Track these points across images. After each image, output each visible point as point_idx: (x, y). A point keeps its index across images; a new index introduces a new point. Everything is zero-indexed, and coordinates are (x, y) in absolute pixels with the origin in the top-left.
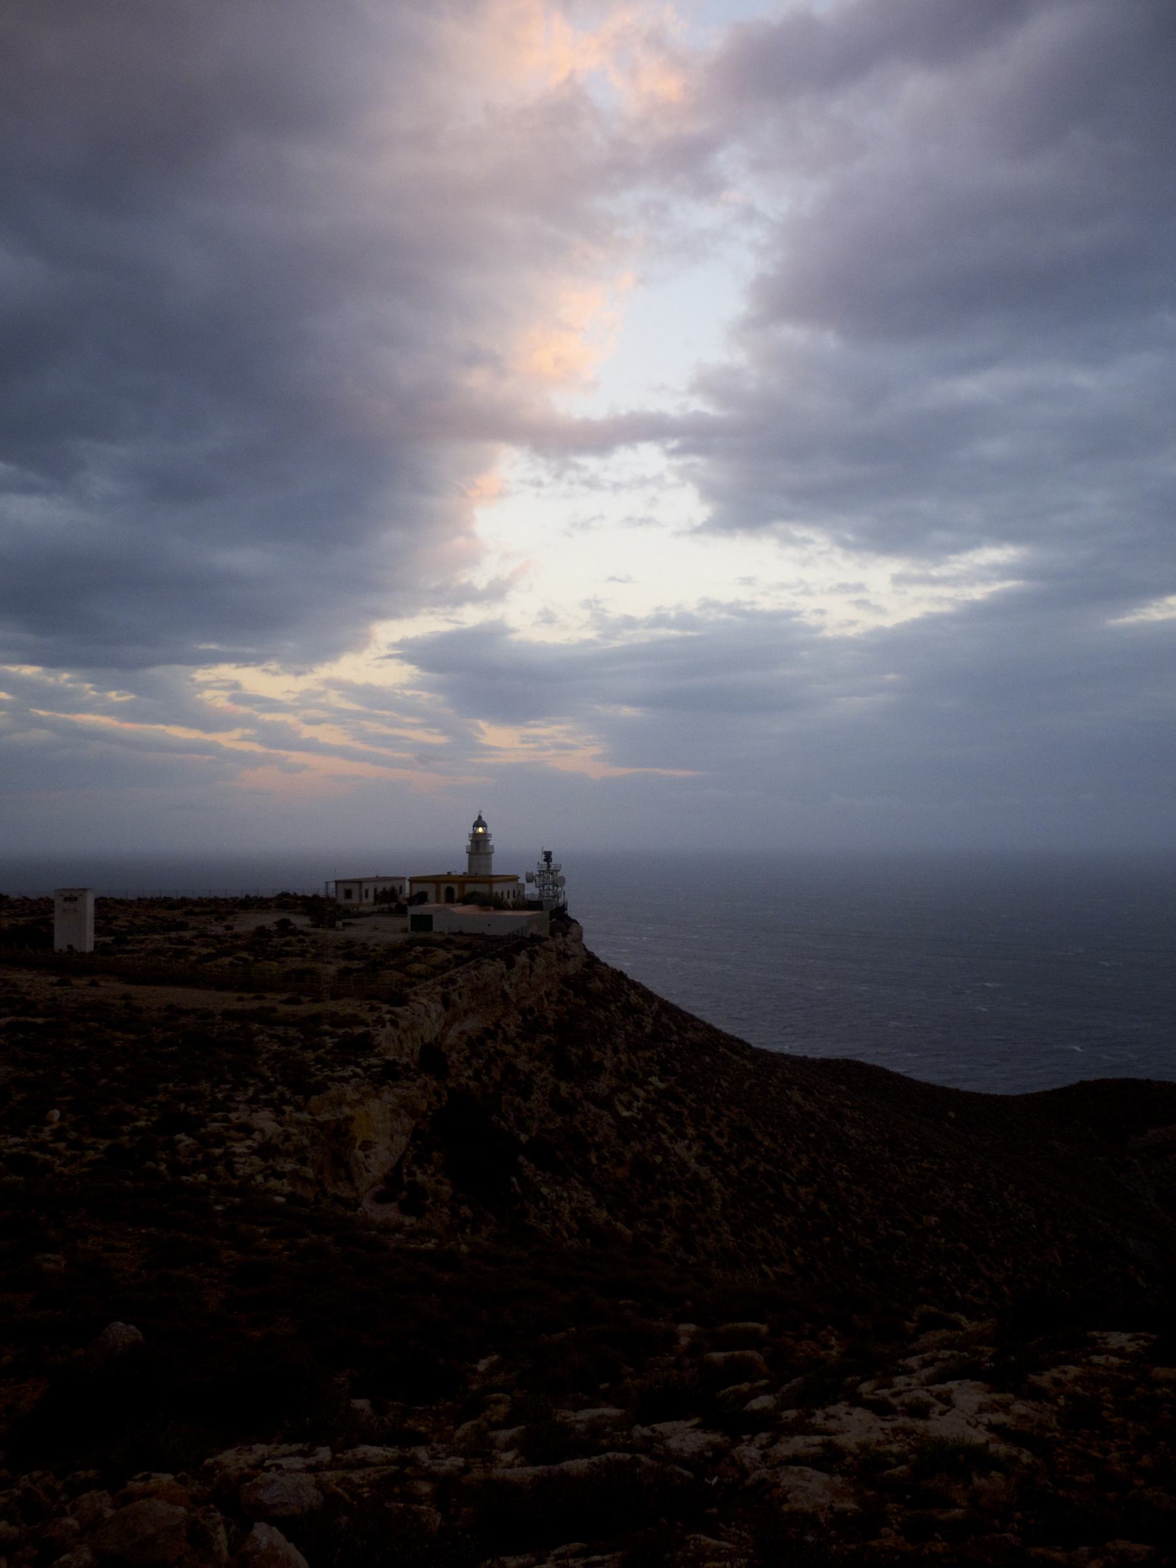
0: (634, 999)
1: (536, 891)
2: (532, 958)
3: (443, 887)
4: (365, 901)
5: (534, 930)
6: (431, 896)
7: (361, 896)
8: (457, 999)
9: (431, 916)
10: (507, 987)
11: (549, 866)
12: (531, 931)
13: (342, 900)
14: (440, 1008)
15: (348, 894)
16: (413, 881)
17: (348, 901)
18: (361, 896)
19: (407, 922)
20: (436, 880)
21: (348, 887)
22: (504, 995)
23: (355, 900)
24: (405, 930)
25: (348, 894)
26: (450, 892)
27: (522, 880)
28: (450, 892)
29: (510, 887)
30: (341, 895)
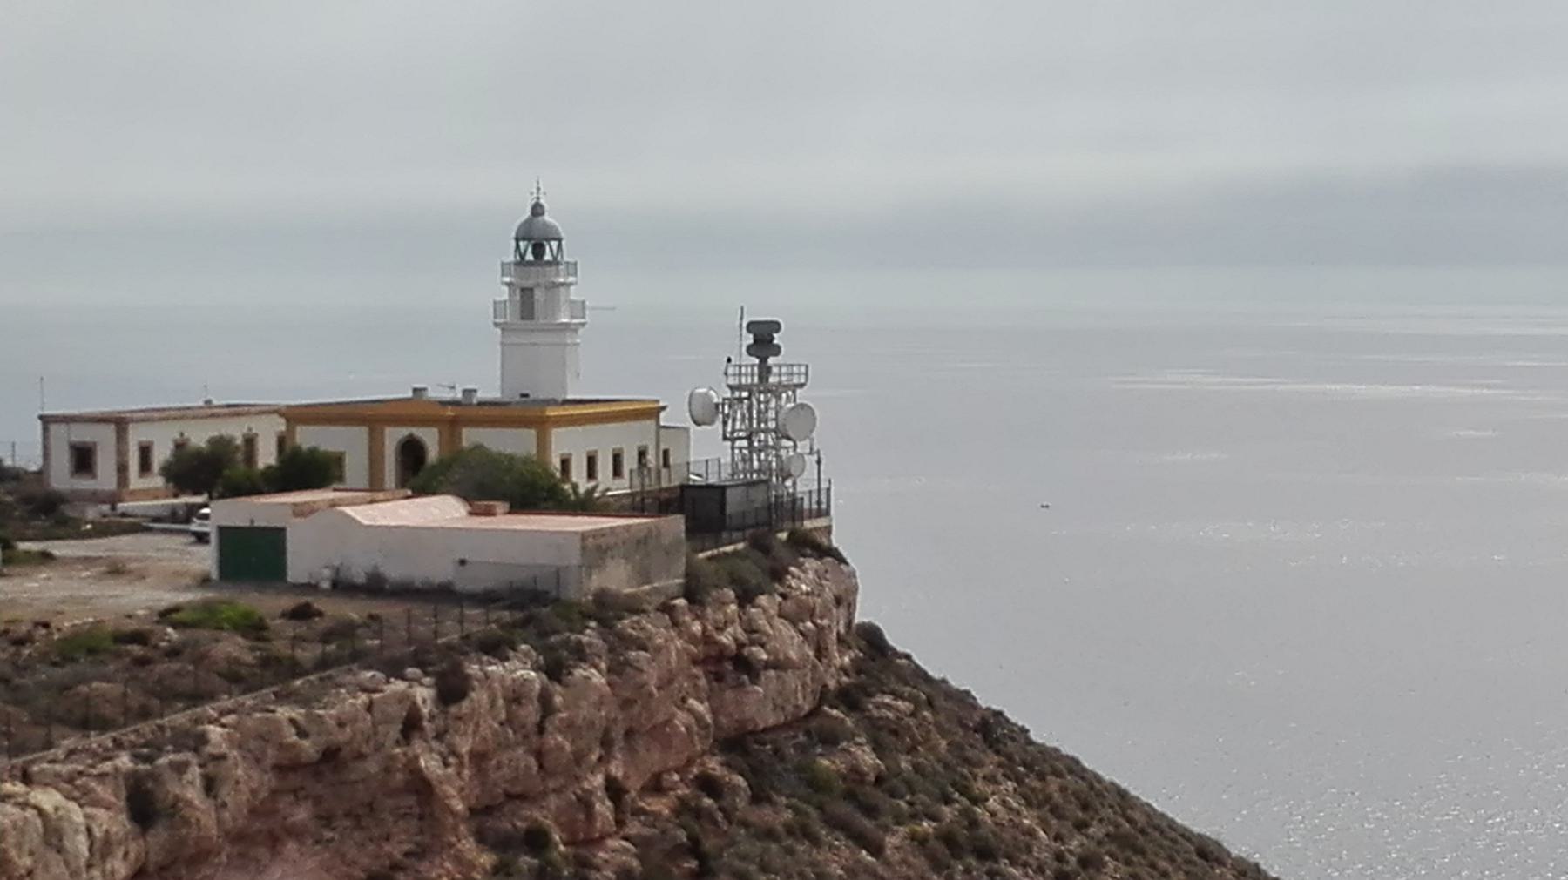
0: (999, 803)
1: (724, 453)
2: (554, 671)
3: (393, 436)
4: (135, 481)
5: (616, 578)
6: (356, 467)
7: (122, 469)
8: (194, 794)
9: (281, 532)
10: (430, 763)
11: (765, 371)
12: (596, 582)
13: (62, 478)
14: (112, 821)
15: (83, 459)
16: (297, 416)
17: (84, 484)
18: (122, 469)
19: (206, 559)
20: (368, 416)
21: (83, 434)
22: (422, 787)
23: (105, 478)
24: (205, 581)
25: (83, 459)
26: (412, 452)
27: (675, 415)
28: (412, 452)
29: (629, 438)
30: (62, 461)
